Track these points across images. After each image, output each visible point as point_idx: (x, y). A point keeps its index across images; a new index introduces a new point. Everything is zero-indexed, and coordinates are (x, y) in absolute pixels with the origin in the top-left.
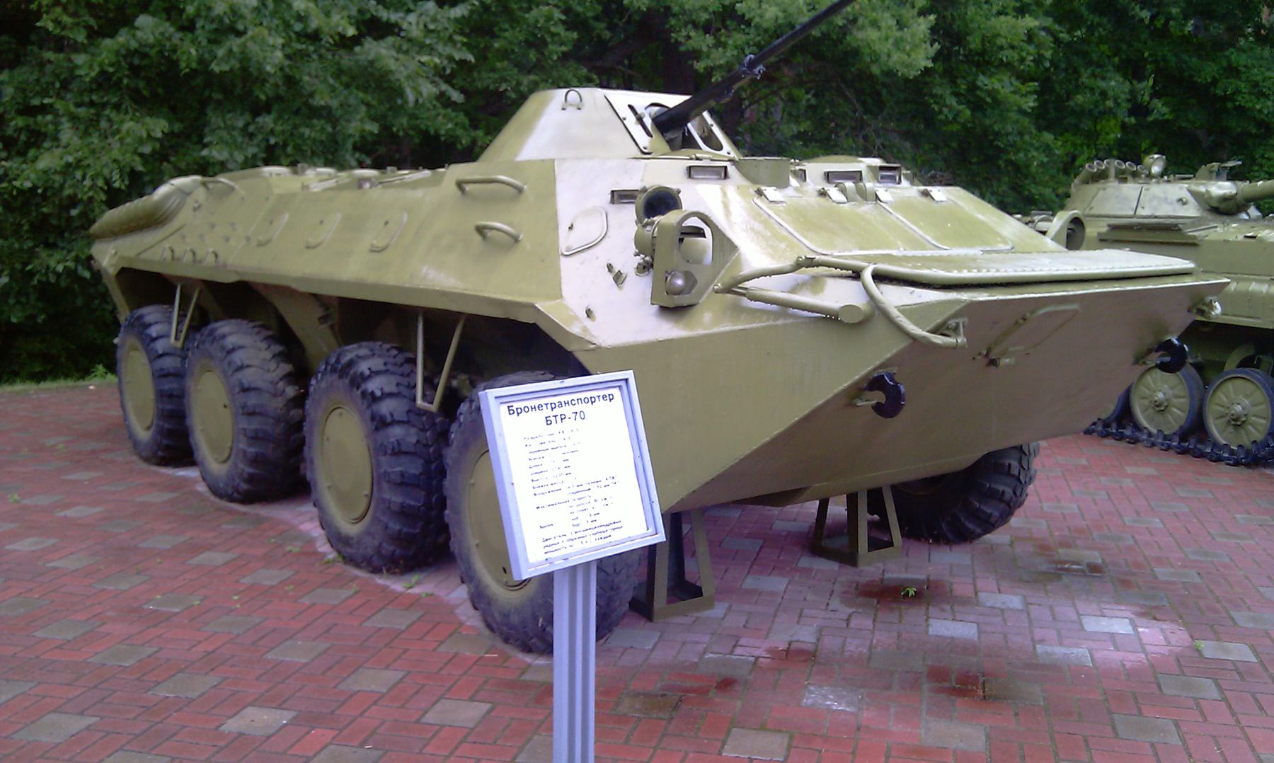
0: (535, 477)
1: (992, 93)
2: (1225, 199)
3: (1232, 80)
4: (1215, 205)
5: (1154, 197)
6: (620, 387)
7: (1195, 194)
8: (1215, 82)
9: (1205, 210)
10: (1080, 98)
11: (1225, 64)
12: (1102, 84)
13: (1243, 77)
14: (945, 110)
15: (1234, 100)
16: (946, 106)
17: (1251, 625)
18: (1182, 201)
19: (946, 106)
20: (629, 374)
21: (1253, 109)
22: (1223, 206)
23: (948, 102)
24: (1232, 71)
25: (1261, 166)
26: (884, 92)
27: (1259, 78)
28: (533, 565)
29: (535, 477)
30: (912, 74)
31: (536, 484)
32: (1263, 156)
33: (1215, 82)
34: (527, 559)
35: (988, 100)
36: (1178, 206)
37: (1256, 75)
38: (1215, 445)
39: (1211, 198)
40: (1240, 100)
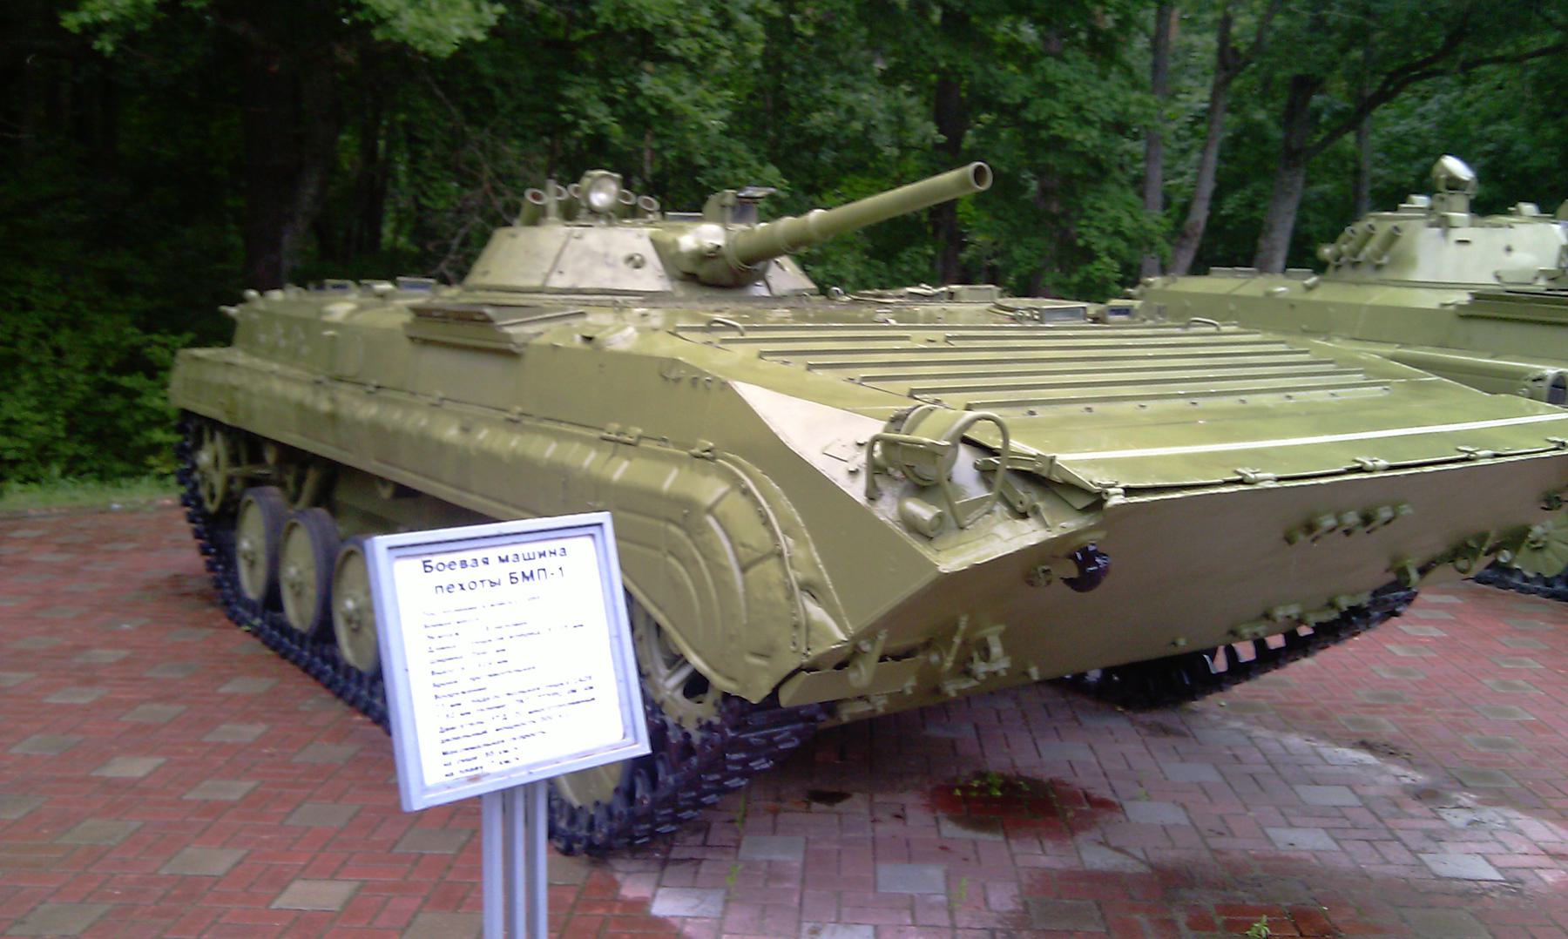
0: (439, 667)
1: (660, 104)
2: (709, 256)
3: (1047, 101)
4: (689, 268)
5: (589, 253)
6: (592, 536)
7: (657, 245)
8: (1025, 103)
9: (672, 278)
10: (817, 118)
11: (1038, 78)
12: (848, 97)
13: (1062, 96)
14: (583, 122)
15: (1047, 128)
16: (586, 117)
17: (1482, 750)
18: (636, 262)
19: (586, 117)
20: (604, 517)
21: (1072, 140)
22: (703, 271)
23: (591, 112)
24: (1048, 89)
25: (1090, 218)
26: (498, 92)
27: (1081, 98)
28: (436, 789)
29: (439, 667)
30: (445, 50)
31: (438, 679)
32: (1092, 207)
33: (1025, 103)
34: (422, 782)
35: (652, 111)
36: (626, 268)
37: (1078, 93)
38: (335, 661)
39: (679, 254)
40: (1057, 129)
